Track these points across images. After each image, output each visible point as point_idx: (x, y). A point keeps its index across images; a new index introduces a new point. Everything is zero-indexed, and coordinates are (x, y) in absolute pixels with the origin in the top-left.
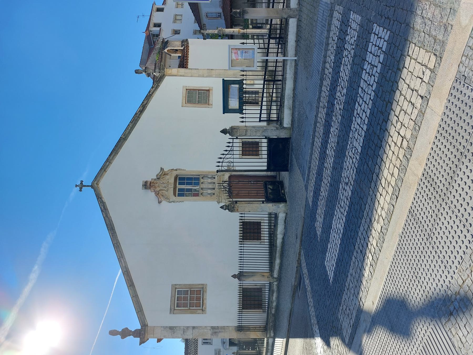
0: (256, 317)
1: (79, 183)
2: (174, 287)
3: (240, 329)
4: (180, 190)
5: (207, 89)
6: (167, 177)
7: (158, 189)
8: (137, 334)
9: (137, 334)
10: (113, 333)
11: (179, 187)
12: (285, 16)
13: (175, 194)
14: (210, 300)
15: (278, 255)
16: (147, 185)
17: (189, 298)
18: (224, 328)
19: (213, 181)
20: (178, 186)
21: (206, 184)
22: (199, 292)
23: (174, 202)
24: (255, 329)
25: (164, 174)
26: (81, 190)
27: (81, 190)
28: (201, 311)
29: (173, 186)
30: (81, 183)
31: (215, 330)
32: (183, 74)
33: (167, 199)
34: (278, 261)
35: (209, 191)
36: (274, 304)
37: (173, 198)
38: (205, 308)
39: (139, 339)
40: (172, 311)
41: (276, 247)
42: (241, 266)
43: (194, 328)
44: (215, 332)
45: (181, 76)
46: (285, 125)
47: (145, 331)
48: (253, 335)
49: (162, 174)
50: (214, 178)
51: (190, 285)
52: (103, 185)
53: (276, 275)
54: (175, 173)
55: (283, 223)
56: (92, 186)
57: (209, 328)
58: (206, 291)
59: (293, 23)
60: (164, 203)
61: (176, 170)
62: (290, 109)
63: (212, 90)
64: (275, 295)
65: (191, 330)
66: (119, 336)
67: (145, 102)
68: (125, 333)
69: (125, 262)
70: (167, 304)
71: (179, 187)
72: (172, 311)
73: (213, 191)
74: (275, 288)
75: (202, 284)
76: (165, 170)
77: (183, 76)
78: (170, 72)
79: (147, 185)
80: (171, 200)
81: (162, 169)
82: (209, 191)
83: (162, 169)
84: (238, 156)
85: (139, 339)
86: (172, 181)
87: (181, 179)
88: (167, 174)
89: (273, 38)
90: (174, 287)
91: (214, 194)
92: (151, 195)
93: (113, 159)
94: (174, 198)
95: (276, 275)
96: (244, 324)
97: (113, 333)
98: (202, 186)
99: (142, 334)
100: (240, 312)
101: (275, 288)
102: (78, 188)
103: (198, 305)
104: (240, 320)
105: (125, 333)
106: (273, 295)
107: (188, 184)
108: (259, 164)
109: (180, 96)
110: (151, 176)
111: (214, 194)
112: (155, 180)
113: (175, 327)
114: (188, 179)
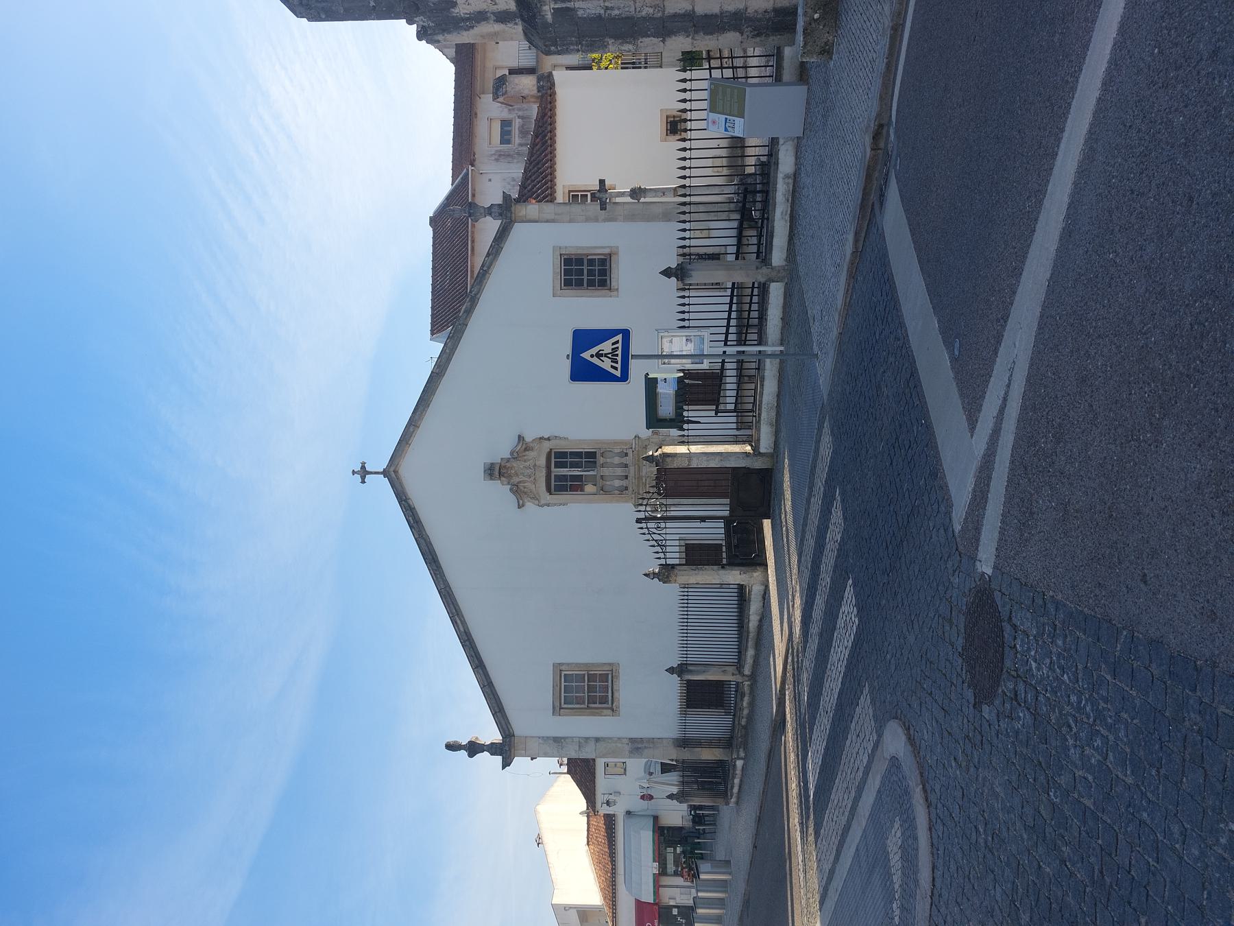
0: (710, 722)
1: (358, 468)
2: (558, 668)
3: (683, 743)
4: (558, 478)
5: (607, 251)
6: (531, 454)
7: (515, 480)
8: (493, 749)
9: (493, 749)
10: (452, 747)
11: (557, 471)
12: (763, 280)
13: (549, 490)
14: (626, 692)
15: (750, 643)
16: (495, 471)
17: (588, 689)
18: (652, 742)
19: (624, 460)
20: (553, 468)
21: (610, 471)
22: (604, 678)
23: (548, 505)
24: (710, 743)
25: (526, 450)
26: (363, 482)
27: (363, 482)
28: (609, 712)
29: (544, 471)
30: (363, 467)
31: (637, 746)
32: (552, 217)
33: (535, 498)
34: (751, 652)
35: (617, 483)
36: (746, 712)
37: (547, 498)
38: (618, 707)
39: (500, 758)
40: (558, 710)
41: (748, 632)
42: (685, 646)
43: (597, 740)
44: (638, 749)
45: (547, 221)
46: (762, 450)
47: (510, 745)
48: (708, 755)
49: (523, 446)
50: (626, 455)
51: (586, 664)
52: (407, 471)
53: (747, 671)
54: (547, 446)
55: (760, 598)
56: (385, 473)
57: (626, 741)
58: (618, 677)
59: (776, 292)
60: (530, 506)
61: (549, 439)
62: (771, 424)
63: (616, 254)
64: (746, 699)
65: (592, 743)
66: (464, 753)
67: (476, 290)
68: (473, 749)
69: (464, 623)
70: (547, 698)
71: (557, 471)
72: (558, 710)
73: (624, 483)
74: (746, 689)
75: (610, 664)
76: (528, 439)
77: (553, 221)
78: (523, 213)
79: (495, 471)
80: (543, 502)
81: (521, 438)
82: (617, 483)
83: (521, 438)
84: (695, 115)
85: (500, 758)
86: (542, 461)
87: (560, 458)
88: (531, 449)
89: (745, 51)
90: (558, 668)
91: (626, 488)
92: (500, 491)
93: (421, 418)
94: (549, 497)
95: (747, 671)
96: (692, 734)
97: (452, 747)
98: (606, 472)
99: (506, 750)
100: (684, 713)
101: (746, 689)
102: (358, 477)
103: (604, 700)
104: (684, 726)
105: (473, 749)
106: (742, 700)
107: (573, 465)
108: (722, 234)
109: (547, 271)
110: (502, 450)
111: (626, 488)
112: (508, 460)
113: (565, 738)
114: (574, 454)
